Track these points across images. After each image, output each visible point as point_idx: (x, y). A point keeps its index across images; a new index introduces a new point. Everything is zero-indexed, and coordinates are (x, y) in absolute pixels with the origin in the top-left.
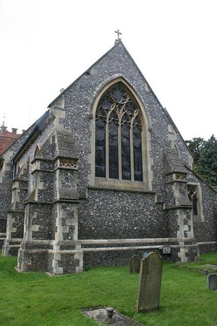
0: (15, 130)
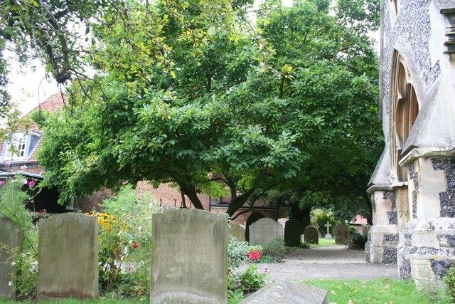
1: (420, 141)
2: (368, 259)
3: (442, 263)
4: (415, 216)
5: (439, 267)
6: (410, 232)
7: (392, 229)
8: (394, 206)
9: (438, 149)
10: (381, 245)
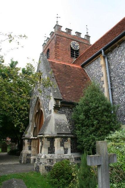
0: (69, 31)
1: (45, 133)
2: (20, 162)
3: (47, 167)
4: (41, 153)
5: (47, 168)
6: (39, 158)
7: (29, 152)
8: (31, 144)
9: (49, 136)
10: (26, 157)
